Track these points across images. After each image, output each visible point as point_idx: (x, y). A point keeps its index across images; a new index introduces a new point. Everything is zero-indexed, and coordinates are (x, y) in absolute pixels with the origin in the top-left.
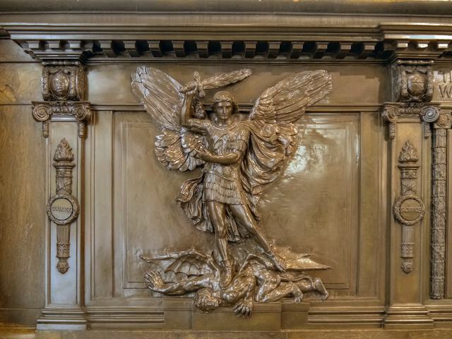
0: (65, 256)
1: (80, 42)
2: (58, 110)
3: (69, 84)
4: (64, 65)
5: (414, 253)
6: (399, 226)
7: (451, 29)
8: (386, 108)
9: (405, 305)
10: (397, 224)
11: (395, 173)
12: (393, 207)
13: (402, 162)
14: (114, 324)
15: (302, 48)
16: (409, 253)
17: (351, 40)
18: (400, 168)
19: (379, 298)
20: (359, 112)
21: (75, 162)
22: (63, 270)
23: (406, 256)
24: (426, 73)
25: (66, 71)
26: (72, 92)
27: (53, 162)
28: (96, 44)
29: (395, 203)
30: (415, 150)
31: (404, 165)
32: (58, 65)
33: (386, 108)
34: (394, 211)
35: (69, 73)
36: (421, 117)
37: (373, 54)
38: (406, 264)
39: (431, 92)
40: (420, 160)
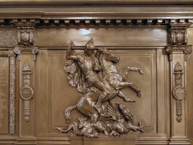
0: (180, 114)
1: (26, 19)
2: (177, 48)
3: (29, 37)
4: (27, 29)
5: (30, 113)
6: (175, 100)
7: (192, 14)
8: (168, 47)
9: (65, 138)
10: (174, 99)
12: (172, 92)
13: (24, 72)
14: (52, 143)
15: (120, 22)
16: (27, 113)
17: (26, 18)
18: (174, 74)
19: (89, 133)
20: (156, 49)
21: (183, 72)
22: (179, 121)
23: (25, 114)
24: (184, 33)
25: (28, 31)
26: (31, 41)
27: (173, 72)
29: (173, 90)
30: (181, 66)
31: (177, 73)
32: (25, 29)
33: (168, 47)
34: (172, 94)
35: (29, 32)
36: (184, 51)
37: (161, 24)
38: (25, 118)
39: (186, 41)
40: (183, 70)
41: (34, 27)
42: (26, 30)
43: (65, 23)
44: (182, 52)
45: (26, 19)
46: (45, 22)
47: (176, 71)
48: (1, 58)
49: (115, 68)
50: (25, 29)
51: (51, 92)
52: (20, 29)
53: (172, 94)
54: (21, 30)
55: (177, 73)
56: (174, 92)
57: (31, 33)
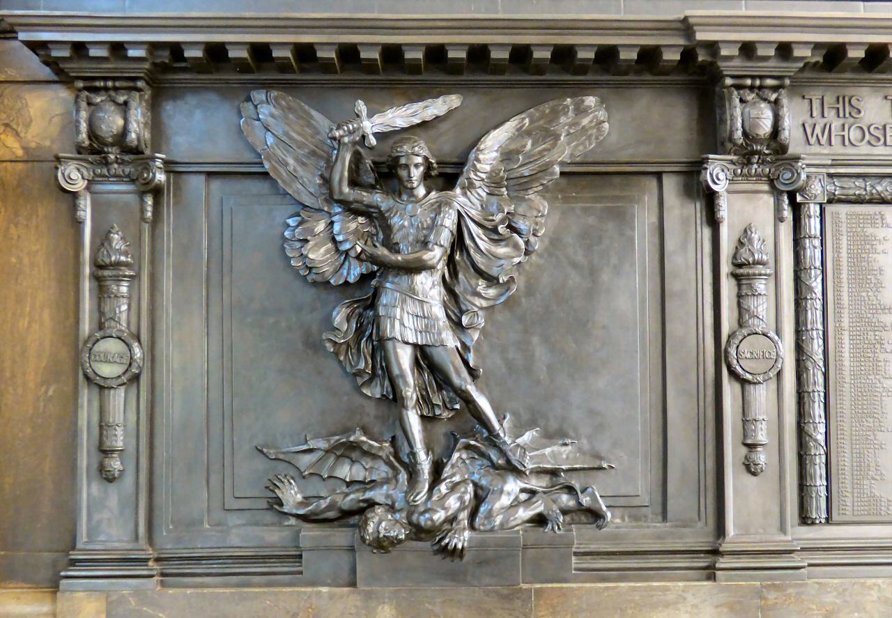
4: (116, 89)
11: (728, 288)
18: (736, 277)
25: (121, 99)
28: (176, 49)
31: (741, 271)
32: (106, 89)
36: (771, 182)
41: (148, 83)
42: (112, 93)
43: (273, 59)
44: (766, 187)
45: (146, 47)
46: (274, 55)
47: (740, 266)
48: (2, 41)
49: (823, 370)
50: (106, 89)
51: (140, 231)
52: (86, 88)
53: (726, 357)
54: (92, 95)
55: (741, 271)
56: (733, 351)
57: (133, 104)
